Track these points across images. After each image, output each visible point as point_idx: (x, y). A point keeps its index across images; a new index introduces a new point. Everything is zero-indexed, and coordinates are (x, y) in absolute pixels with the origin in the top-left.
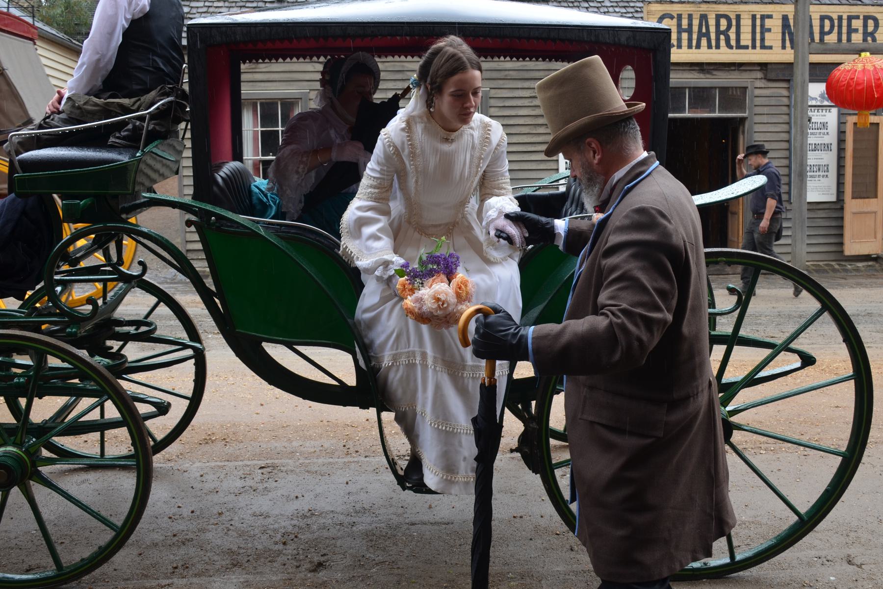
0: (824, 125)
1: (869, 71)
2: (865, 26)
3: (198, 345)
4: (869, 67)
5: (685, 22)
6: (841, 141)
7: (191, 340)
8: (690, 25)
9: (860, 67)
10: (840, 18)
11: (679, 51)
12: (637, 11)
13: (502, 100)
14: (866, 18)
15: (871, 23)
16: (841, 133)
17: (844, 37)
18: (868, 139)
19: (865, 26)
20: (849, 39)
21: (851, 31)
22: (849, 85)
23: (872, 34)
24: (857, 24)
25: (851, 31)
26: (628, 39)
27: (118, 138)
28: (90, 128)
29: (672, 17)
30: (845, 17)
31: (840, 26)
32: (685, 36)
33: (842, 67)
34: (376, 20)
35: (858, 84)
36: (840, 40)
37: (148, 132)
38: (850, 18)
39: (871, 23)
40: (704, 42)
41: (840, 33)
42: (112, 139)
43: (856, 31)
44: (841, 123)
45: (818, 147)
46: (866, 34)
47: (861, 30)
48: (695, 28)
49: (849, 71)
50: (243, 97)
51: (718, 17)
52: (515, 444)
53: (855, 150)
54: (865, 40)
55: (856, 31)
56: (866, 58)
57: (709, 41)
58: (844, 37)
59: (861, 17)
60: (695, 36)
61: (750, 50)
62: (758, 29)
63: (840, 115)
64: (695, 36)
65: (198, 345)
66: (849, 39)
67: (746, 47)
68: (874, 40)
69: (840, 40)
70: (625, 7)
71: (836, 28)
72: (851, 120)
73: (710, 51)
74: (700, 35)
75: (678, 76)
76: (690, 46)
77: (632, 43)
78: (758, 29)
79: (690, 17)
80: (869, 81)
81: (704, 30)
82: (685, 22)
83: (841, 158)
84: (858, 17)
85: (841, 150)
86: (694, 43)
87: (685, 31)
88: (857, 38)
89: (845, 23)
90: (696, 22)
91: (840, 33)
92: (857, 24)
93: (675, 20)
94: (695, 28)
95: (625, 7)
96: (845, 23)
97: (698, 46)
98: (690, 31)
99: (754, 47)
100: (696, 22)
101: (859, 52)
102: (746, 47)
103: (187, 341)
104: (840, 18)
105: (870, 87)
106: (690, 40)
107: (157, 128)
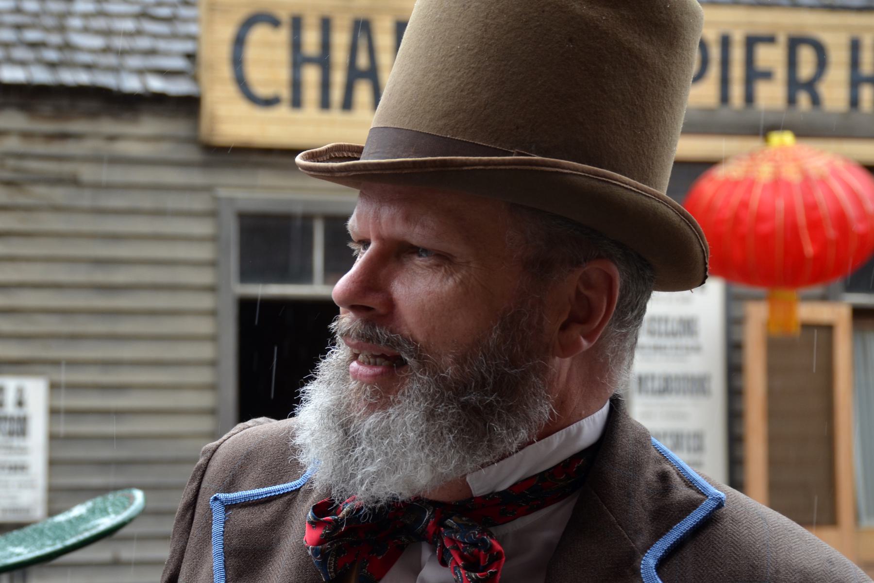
0: (688, 326)
1: (788, 185)
2: (792, 63)
4: (791, 174)
5: (311, 40)
6: (734, 369)
8: (326, 45)
9: (765, 172)
10: (725, 42)
11: (297, 115)
14: (794, 43)
15: (806, 56)
16: (734, 348)
17: (737, 91)
18: (804, 362)
19: (792, 63)
20: (749, 98)
21: (754, 75)
22: (737, 219)
23: (810, 86)
24: (771, 57)
25: (754, 75)
28: (273, 361)
29: (274, 22)
30: (738, 37)
31: (725, 63)
32: (311, 75)
33: (721, 173)
35: (760, 218)
36: (725, 97)
38: (752, 42)
39: (806, 56)
40: (363, 92)
41: (725, 82)
43: (767, 75)
44: (733, 323)
45: (674, 385)
46: (794, 85)
47: (781, 73)
48: (339, 56)
49: (736, 183)
51: (794, 43)
53: (772, 394)
54: (792, 100)
55: (767, 75)
56: (783, 149)
57: (325, 86)
58: (737, 91)
59: (782, 39)
60: (338, 78)
61: (283, 111)
62: (737, 71)
63: (731, 300)
64: (338, 78)
66: (749, 98)
67: (270, 102)
68: (816, 100)
69: (725, 97)
71: (714, 71)
72: (757, 314)
73: (326, 116)
74: (354, 74)
76: (325, 103)
78: (737, 71)
79: (326, 25)
80: (790, 211)
81: (363, 61)
82: (311, 40)
83: (734, 416)
84: (770, 40)
85: (734, 393)
86: (337, 94)
87: (310, 60)
88: (771, 95)
89: (738, 54)
90: (341, 40)
91: (725, 82)
92: (771, 57)
94: (339, 56)
96: (738, 54)
97: (348, 104)
98: (324, 61)
99: (297, 102)
100: (341, 40)
101: (762, 130)
102: (270, 102)
104: (725, 42)
105: (792, 228)
106: (325, 86)
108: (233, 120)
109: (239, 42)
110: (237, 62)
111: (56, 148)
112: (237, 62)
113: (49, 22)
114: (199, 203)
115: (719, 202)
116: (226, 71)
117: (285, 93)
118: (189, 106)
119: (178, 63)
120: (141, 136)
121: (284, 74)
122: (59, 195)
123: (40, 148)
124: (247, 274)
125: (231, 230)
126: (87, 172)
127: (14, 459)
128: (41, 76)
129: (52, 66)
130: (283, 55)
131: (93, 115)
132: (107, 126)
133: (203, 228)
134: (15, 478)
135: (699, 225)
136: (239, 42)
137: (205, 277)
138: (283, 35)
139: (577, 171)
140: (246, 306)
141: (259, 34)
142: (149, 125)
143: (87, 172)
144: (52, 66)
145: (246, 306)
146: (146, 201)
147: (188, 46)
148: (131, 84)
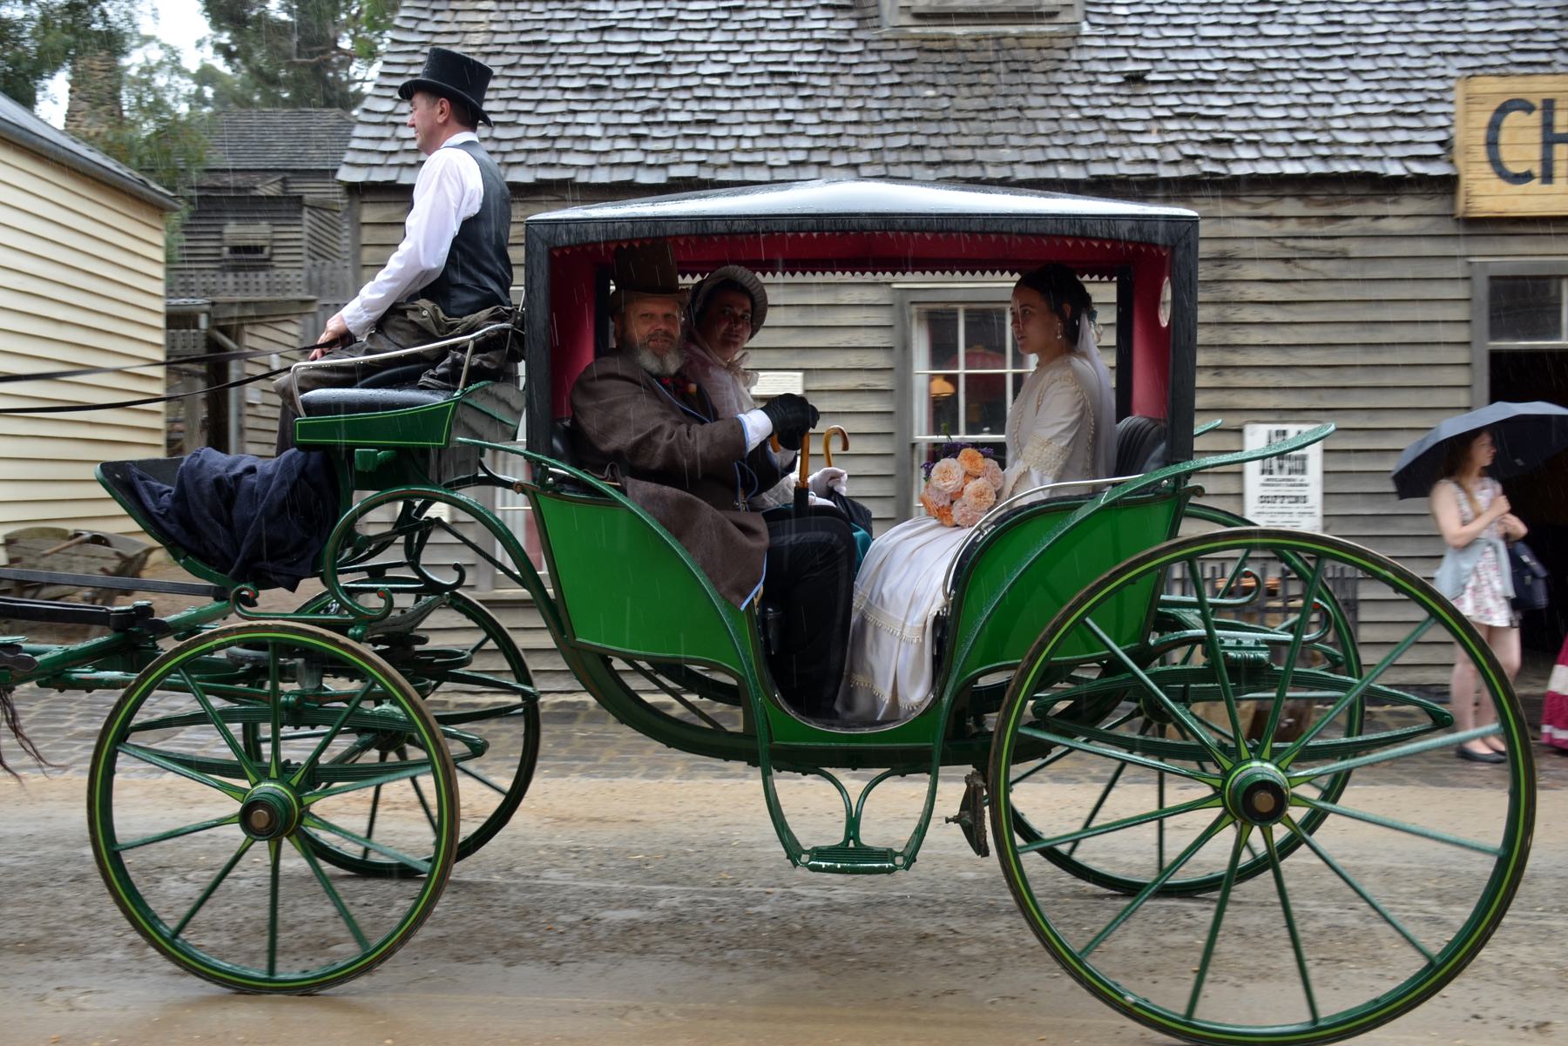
3: (530, 689)
7: (519, 681)
12: (1430, 101)
13: (1360, 285)
26: (1131, 230)
27: (432, 377)
29: (1529, 108)
34: (748, 212)
37: (471, 369)
42: (424, 379)
50: (542, 711)
52: (955, 810)
65: (530, 689)
67: (1527, 177)
70: (1399, 91)
75: (1535, 250)
77: (1137, 237)
93: (1536, 116)
95: (1399, 91)
102: (1527, 177)
103: (512, 682)
107: (485, 364)
108: (1487, 194)
109: (1494, 126)
110: (1492, 144)
111: (1328, 229)
112: (1492, 144)
113: (1316, 125)
114: (1456, 269)
115: (42, 83)
116: (1481, 153)
117: (1537, 170)
118: (1448, 185)
119: (1435, 150)
120: (1399, 214)
121: (1536, 153)
122: (1330, 268)
123: (1315, 230)
124: (1495, 333)
125: (1482, 289)
126: (1355, 248)
127: (1296, 492)
128: (1317, 168)
129: (1324, 158)
130: (1536, 136)
131: (1360, 199)
132: (1374, 208)
133: (1460, 291)
134: (1300, 507)
135: (1013, 30)
136: (1494, 126)
137: (1461, 334)
138: (1536, 118)
139: (393, 935)
140: (1496, 357)
141: (1514, 118)
142: (1410, 205)
143: (1355, 248)
144: (1324, 158)
145: (1496, 357)
146: (1408, 270)
147: (1442, 136)
148: (1396, 170)
